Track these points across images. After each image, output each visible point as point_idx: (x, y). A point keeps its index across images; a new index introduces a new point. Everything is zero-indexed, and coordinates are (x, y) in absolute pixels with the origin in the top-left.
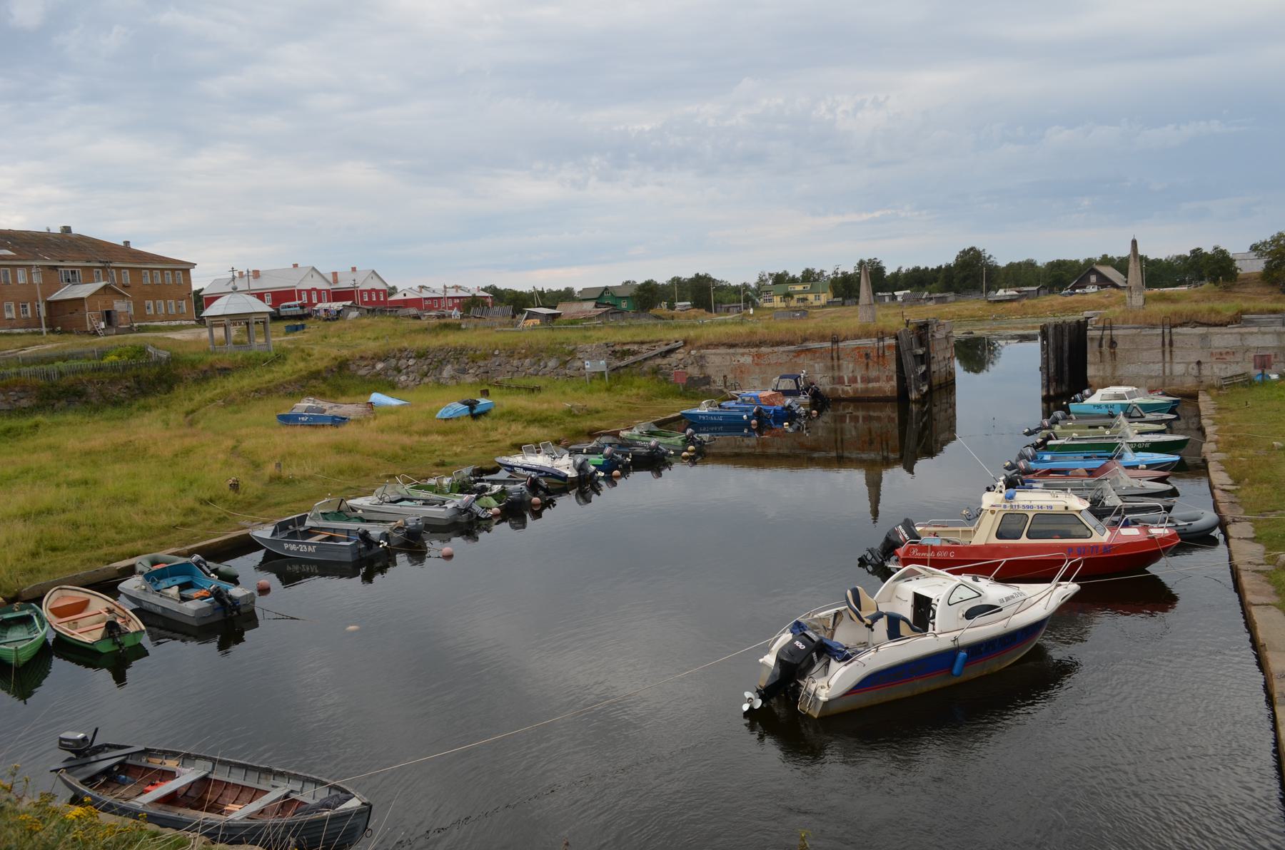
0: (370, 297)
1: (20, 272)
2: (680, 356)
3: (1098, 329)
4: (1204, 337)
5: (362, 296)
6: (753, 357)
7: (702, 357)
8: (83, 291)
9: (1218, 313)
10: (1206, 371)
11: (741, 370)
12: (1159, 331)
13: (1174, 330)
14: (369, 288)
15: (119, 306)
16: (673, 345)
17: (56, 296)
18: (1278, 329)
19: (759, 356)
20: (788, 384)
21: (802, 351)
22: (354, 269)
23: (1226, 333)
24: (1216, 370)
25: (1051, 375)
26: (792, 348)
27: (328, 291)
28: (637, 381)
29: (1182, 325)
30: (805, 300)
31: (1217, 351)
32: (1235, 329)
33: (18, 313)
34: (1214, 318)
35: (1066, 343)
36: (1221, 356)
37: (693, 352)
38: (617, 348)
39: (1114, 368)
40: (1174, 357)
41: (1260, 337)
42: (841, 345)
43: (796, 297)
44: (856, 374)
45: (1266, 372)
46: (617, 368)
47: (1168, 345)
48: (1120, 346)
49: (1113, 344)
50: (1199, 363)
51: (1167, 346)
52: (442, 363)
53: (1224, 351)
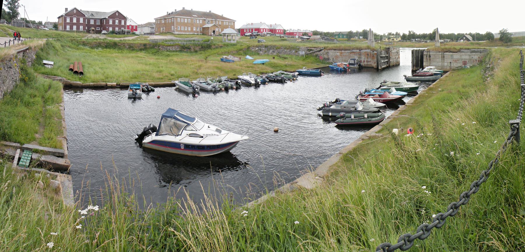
0: (279, 31)
1: (198, 20)
2: (323, 52)
3: (426, 52)
4: (452, 55)
7: (328, 52)
8: (209, 25)
9: (456, 49)
10: (452, 65)
11: (337, 57)
12: (441, 53)
13: (445, 53)
15: (217, 30)
16: (321, 49)
17: (204, 26)
18: (469, 54)
19: (341, 53)
20: (352, 62)
21: (352, 52)
22: (276, 24)
24: (455, 65)
26: (349, 51)
27: (268, 29)
28: (312, 58)
29: (447, 52)
30: (393, 40)
32: (459, 54)
33: (196, 30)
34: (455, 51)
35: (420, 55)
36: (456, 61)
37: (326, 51)
38: (309, 48)
41: (465, 56)
42: (362, 51)
43: (391, 39)
45: (466, 66)
46: (308, 54)
47: (443, 57)
48: (431, 57)
49: (430, 56)
50: (450, 63)
51: (443, 58)
52: (270, 49)
53: (456, 60)
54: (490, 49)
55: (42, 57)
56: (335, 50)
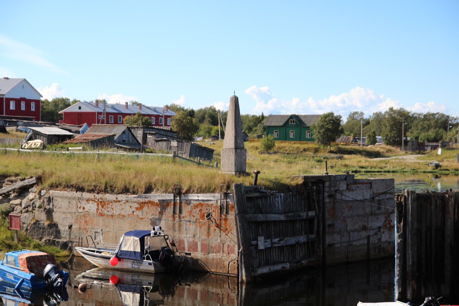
5: (8, 105)
6: (98, 205)
14: (18, 97)
19: (102, 203)
25: (409, 269)
44: (197, 240)
56: (80, 189)
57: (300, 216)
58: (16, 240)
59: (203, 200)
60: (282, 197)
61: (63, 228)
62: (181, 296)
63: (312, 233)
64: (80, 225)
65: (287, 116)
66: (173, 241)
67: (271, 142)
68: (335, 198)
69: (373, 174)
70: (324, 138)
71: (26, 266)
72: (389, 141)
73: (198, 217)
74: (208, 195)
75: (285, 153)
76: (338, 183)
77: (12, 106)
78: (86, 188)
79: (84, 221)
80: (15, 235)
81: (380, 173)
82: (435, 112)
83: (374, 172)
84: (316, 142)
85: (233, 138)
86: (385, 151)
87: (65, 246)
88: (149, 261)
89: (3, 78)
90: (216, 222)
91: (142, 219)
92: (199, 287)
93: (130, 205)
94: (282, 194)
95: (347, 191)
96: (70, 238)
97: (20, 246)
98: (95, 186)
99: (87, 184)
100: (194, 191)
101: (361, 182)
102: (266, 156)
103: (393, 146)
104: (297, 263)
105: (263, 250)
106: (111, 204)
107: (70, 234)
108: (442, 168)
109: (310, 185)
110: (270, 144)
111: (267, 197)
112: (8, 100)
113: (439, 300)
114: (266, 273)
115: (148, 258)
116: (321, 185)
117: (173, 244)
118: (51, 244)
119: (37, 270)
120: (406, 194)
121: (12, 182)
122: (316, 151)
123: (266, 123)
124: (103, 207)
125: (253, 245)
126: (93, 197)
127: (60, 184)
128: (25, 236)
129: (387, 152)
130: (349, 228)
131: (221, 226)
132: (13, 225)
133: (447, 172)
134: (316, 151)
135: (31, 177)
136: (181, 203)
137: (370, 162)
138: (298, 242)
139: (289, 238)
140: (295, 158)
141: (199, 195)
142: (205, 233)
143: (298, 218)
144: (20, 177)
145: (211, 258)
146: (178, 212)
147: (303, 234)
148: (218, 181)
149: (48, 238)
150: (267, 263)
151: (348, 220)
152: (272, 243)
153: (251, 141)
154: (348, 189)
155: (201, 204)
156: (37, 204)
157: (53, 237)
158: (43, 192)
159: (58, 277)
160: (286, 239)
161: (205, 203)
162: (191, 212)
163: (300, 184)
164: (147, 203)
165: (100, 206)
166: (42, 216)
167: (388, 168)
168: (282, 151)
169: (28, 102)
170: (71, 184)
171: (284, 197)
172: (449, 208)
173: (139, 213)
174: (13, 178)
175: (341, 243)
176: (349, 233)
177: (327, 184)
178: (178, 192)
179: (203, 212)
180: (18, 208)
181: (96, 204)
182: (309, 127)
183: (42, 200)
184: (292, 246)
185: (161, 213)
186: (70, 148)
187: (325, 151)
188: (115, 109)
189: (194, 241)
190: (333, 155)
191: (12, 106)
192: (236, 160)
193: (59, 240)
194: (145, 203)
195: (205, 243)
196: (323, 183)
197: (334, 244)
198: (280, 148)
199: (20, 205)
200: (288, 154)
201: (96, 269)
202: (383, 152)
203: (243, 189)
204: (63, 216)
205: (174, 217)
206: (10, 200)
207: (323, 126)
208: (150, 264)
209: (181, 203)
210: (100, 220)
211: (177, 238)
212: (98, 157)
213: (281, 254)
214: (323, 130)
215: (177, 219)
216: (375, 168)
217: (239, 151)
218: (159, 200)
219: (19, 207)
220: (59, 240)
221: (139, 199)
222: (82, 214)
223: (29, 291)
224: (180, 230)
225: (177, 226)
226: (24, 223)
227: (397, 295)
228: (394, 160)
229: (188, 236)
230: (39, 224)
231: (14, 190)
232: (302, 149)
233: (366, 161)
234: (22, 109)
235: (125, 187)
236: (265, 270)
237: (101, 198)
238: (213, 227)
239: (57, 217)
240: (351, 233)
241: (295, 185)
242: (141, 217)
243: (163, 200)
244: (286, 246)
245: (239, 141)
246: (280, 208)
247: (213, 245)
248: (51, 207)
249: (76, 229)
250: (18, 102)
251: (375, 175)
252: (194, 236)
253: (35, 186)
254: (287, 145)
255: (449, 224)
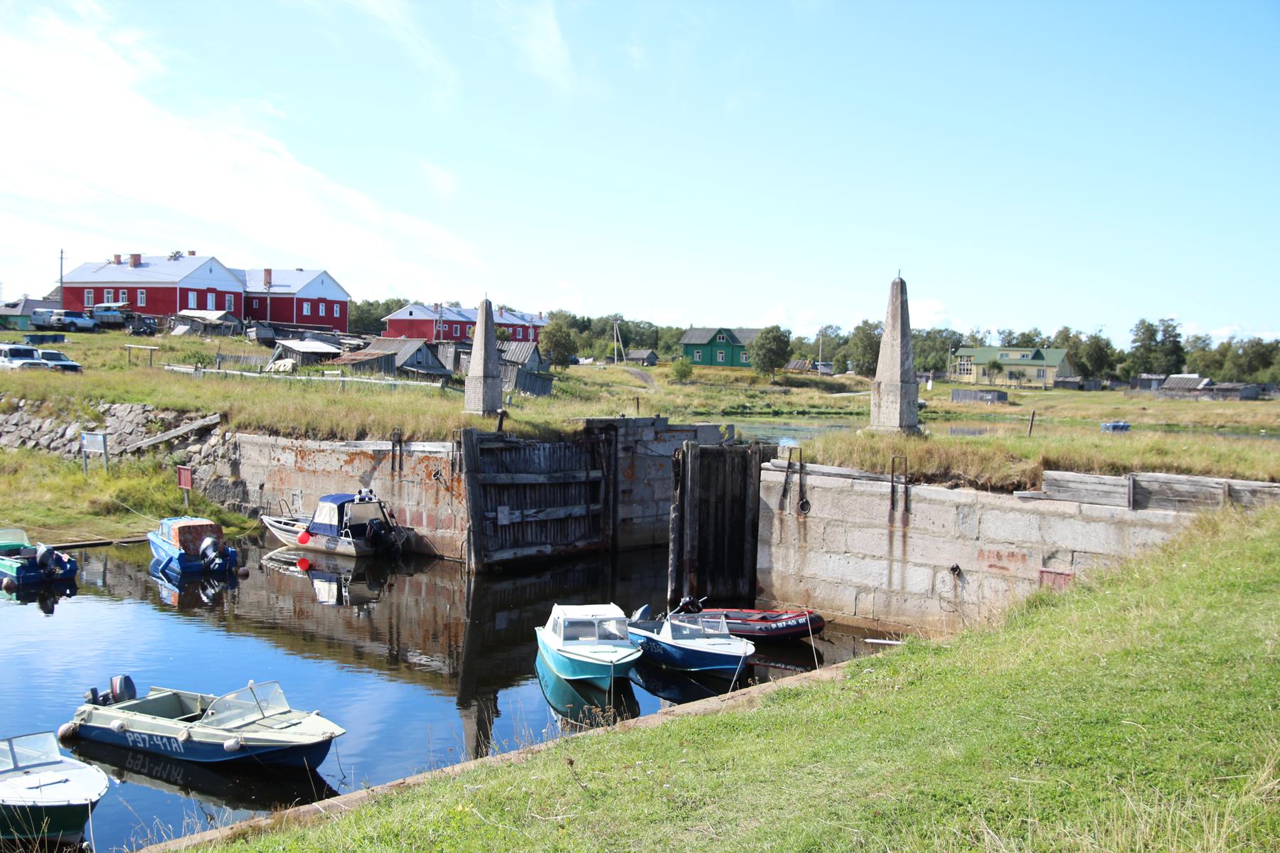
5: (300, 308)
6: (296, 456)
13: (916, 490)
14: (315, 297)
19: (302, 453)
23: (1012, 509)
25: (686, 557)
29: (930, 479)
31: (994, 548)
39: (803, 561)
40: (909, 549)
41: (1078, 525)
50: (956, 570)
53: (1005, 550)
54: (731, 428)
55: (1208, 469)
56: (274, 432)
57: (574, 477)
58: (186, 502)
59: (430, 452)
60: (547, 450)
61: (252, 488)
62: (402, 590)
63: (595, 501)
64: (274, 484)
65: (714, 329)
66: (391, 511)
67: (687, 366)
68: (633, 453)
69: (829, 416)
70: (764, 363)
71: (177, 539)
72: (861, 369)
73: (424, 476)
74: (437, 444)
75: (707, 384)
76: (640, 430)
77: (306, 310)
78: (282, 431)
79: (278, 478)
80: (186, 495)
81: (838, 416)
82: (943, 329)
83: (829, 413)
84: (753, 368)
85: (482, 362)
86: (853, 383)
87: (254, 513)
88: (348, 539)
89: (294, 269)
90: (446, 484)
91: (352, 477)
92: (423, 578)
93: (337, 456)
94: (547, 445)
95: (655, 443)
96: (261, 502)
97: (190, 511)
98: (294, 429)
99: (284, 425)
100: (419, 438)
101: (678, 429)
102: (678, 387)
103: (867, 376)
104: (567, 545)
105: (505, 526)
106: (313, 454)
107: (261, 497)
108: (928, 410)
109: (596, 431)
110: (684, 370)
111: (520, 449)
112: (301, 301)
113: (701, 602)
114: (508, 560)
115: (347, 535)
116: (613, 433)
117: (392, 516)
118: (235, 511)
119: (194, 545)
120: (685, 449)
121: (191, 419)
122: (754, 381)
123: (685, 340)
124: (302, 458)
125: (489, 519)
126: (290, 444)
127: (250, 424)
128: (201, 499)
129: (856, 385)
130: (657, 496)
131: (452, 489)
132: (183, 482)
133: (934, 415)
134: (754, 381)
135: (215, 414)
136: (401, 455)
137: (826, 399)
138: (570, 515)
139: (554, 509)
140: (720, 392)
141: (425, 444)
142: (433, 499)
143: (571, 480)
144: (200, 414)
145: (439, 535)
146: (397, 468)
147: (582, 503)
148: (451, 424)
149: (233, 501)
150: (516, 544)
151: (657, 485)
152: (523, 516)
153: (660, 365)
154: (656, 439)
155: (427, 458)
156: (220, 452)
157: (239, 500)
158: (228, 435)
159: (216, 557)
160: (549, 510)
161: (433, 455)
162: (414, 468)
163: (581, 431)
164: (359, 454)
165: (299, 456)
166: (225, 470)
167: (852, 407)
168: (702, 380)
169: (330, 304)
170: (264, 424)
171: (550, 449)
172: (751, 469)
173: (347, 468)
174: (193, 415)
175: (643, 517)
176: (657, 502)
177: (621, 431)
178: (398, 440)
179: (430, 469)
180: (197, 458)
181: (294, 454)
182: (743, 346)
183: (226, 447)
184: (563, 522)
185: (374, 469)
186: (326, 372)
187: (766, 382)
188: (462, 315)
189: (417, 511)
190: (777, 388)
191: (306, 310)
192: (485, 394)
193: (247, 505)
194: (356, 454)
195: (432, 513)
196: (616, 429)
197: (631, 519)
198: (700, 376)
199: (200, 453)
200: (712, 385)
201: (284, 548)
202: (850, 385)
203: (475, 437)
204: (253, 470)
205: (393, 476)
206: (188, 445)
207: (763, 345)
208: (349, 543)
209: (401, 455)
210: (299, 478)
211: (396, 505)
212: (343, 386)
213: (542, 532)
214: (764, 351)
215: (397, 478)
216: (832, 408)
217: (489, 381)
218: (374, 451)
219: (198, 455)
220: (247, 505)
221: (347, 448)
222: (276, 469)
223: (178, 574)
224: (400, 495)
225: (396, 488)
226: (202, 480)
227: (299, 583)
228: (862, 397)
229: (410, 503)
230: (221, 481)
231: (191, 431)
232: (732, 379)
233: (820, 398)
234: (321, 314)
235: (332, 430)
236: (507, 555)
237: (301, 446)
238: (442, 488)
239: (245, 472)
240: (661, 504)
241: (572, 431)
242: (351, 474)
243: (379, 451)
244: (551, 520)
245: (490, 366)
246: (542, 464)
247: (443, 517)
248: (238, 457)
249: (269, 490)
250: (315, 303)
251: (832, 418)
252: (418, 504)
253: (219, 426)
254: (711, 372)
255: (751, 492)
